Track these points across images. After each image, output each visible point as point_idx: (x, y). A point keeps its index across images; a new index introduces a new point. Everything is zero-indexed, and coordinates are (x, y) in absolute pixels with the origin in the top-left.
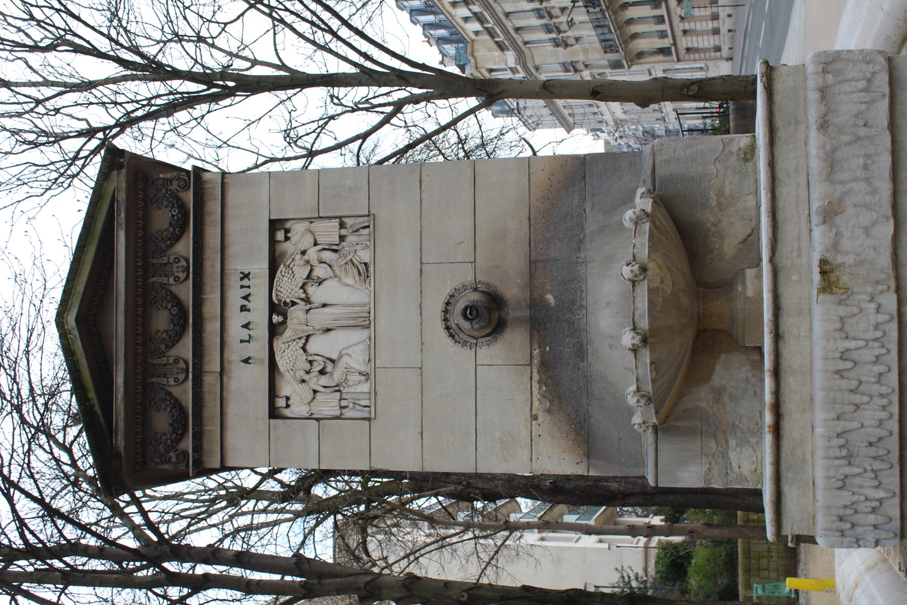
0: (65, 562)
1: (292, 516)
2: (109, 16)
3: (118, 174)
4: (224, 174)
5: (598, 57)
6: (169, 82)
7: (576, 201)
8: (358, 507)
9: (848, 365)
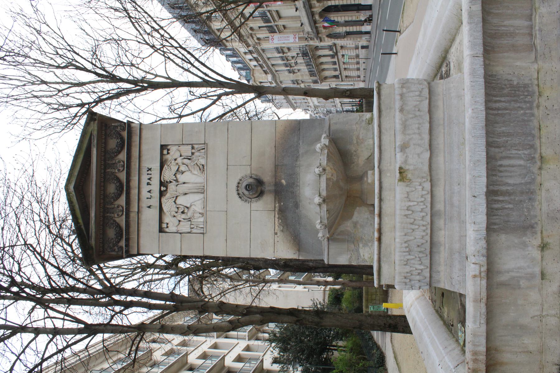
0: (69, 295)
1: (169, 276)
2: (92, 54)
3: (94, 123)
4: (141, 124)
5: (308, 78)
6: (118, 84)
7: (296, 140)
8: (199, 272)
9: (410, 212)
